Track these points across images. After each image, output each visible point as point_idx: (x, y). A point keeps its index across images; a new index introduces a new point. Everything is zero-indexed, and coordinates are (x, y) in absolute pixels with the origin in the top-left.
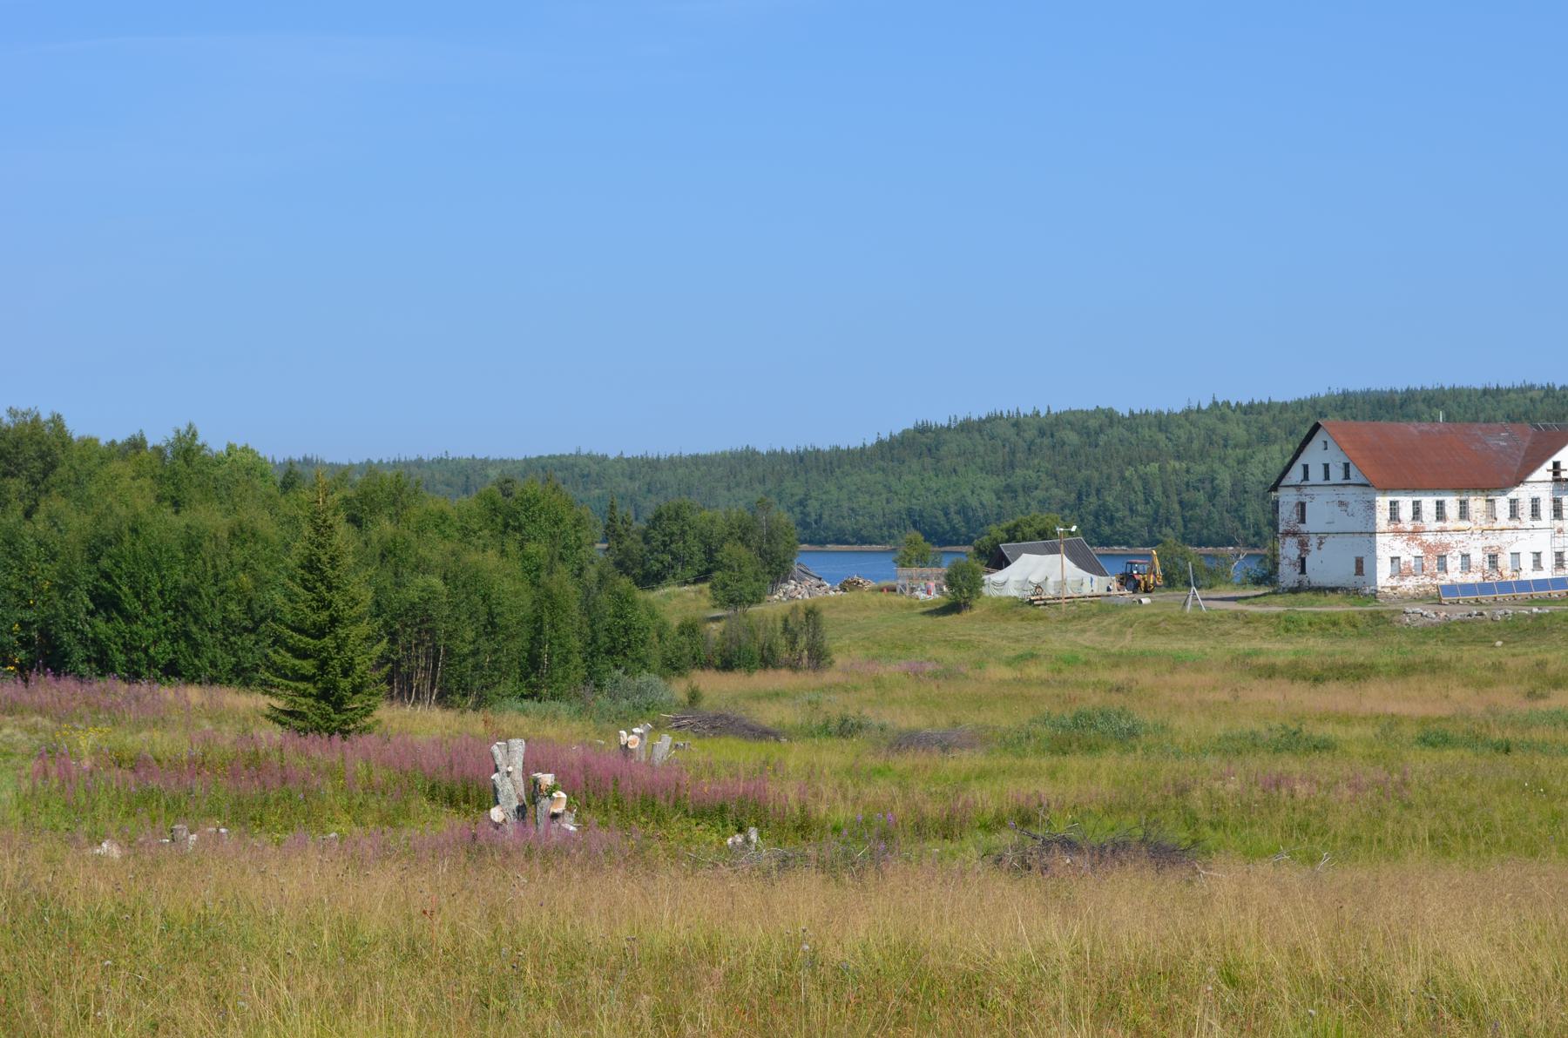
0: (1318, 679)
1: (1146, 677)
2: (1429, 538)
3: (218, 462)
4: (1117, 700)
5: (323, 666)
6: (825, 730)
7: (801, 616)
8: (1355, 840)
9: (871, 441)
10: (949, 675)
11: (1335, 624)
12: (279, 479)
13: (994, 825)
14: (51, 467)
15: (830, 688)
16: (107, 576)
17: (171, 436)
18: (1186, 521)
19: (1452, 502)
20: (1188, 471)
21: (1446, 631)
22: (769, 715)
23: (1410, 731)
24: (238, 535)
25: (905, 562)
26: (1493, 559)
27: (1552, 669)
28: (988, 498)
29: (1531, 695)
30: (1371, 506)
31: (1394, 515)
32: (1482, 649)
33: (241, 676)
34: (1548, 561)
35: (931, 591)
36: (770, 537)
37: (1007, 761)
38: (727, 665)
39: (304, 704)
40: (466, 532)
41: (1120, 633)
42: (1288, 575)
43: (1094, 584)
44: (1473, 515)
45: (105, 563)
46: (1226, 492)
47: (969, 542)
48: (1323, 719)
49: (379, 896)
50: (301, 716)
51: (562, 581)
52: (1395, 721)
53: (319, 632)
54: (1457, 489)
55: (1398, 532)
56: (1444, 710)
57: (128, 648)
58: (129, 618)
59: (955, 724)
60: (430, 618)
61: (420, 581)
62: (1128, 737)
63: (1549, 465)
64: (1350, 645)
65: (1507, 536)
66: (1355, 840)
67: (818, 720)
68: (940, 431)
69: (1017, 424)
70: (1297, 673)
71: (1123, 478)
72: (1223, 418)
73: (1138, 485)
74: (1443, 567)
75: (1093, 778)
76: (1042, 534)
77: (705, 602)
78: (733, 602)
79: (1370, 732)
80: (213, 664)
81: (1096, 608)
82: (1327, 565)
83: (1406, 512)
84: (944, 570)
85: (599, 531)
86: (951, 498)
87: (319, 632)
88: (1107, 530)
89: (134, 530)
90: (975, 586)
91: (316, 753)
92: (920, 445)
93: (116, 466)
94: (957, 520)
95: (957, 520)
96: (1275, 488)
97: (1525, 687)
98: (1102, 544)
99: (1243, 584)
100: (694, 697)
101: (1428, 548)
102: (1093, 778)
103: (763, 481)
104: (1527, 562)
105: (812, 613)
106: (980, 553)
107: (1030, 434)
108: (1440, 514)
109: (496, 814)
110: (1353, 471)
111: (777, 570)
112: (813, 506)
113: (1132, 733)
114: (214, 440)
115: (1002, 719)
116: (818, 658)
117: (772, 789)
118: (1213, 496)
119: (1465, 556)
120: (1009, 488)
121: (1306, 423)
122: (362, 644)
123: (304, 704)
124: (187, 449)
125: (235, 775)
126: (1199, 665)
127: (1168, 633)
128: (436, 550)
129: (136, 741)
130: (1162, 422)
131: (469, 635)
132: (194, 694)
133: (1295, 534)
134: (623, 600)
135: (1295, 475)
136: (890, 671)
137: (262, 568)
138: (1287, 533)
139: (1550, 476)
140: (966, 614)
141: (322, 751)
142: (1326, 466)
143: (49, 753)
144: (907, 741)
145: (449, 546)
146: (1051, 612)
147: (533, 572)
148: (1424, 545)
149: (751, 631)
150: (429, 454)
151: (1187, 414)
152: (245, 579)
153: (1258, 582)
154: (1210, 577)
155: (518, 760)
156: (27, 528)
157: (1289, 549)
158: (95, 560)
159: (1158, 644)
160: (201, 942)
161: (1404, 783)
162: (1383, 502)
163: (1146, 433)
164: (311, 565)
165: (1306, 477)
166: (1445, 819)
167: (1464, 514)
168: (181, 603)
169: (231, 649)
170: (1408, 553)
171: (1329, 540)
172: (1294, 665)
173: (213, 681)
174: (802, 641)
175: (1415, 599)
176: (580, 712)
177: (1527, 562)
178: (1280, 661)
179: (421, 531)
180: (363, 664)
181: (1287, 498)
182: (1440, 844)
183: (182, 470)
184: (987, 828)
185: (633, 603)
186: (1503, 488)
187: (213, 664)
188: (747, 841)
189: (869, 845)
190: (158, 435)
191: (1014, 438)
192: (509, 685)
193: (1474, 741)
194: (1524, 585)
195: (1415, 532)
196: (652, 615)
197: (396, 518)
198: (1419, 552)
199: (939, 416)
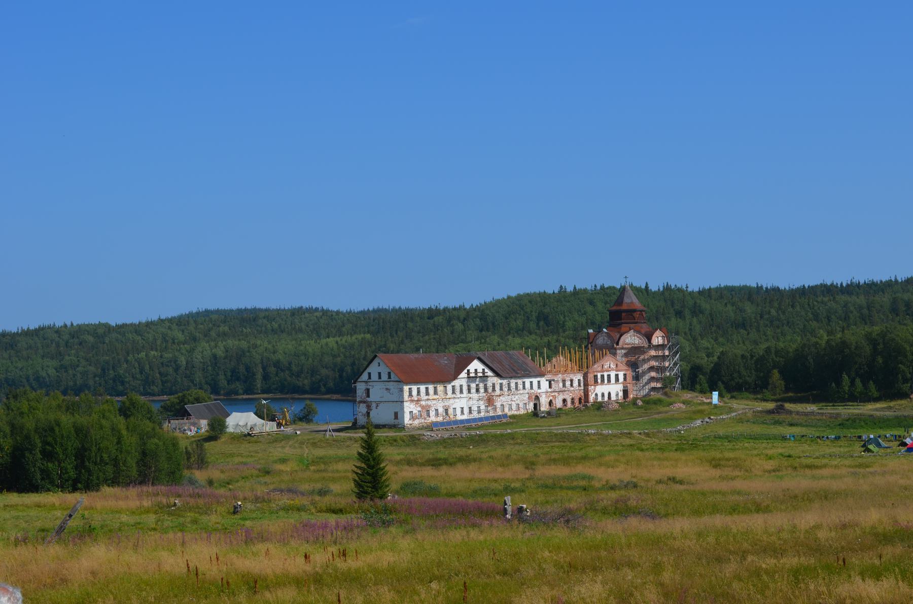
2: (423, 403)
11: (395, 441)
18: (163, 383)
19: (431, 388)
20: (161, 357)
26: (446, 411)
30: (402, 390)
31: (410, 395)
34: (466, 411)
44: (439, 393)
46: (183, 368)
54: (433, 382)
55: (412, 401)
63: (466, 371)
65: (451, 401)
68: (14, 336)
69: (58, 331)
71: (127, 361)
73: (137, 365)
81: (275, 439)
83: (415, 393)
86: (30, 372)
98: (118, 395)
101: (423, 407)
104: (458, 412)
107: (66, 337)
108: (427, 393)
110: (392, 376)
118: (177, 369)
119: (437, 410)
120: (62, 366)
133: (364, 402)
138: (360, 402)
139: (466, 376)
142: (380, 373)
163: (130, 336)
165: (370, 377)
167: (436, 393)
170: (416, 410)
171: (381, 405)
177: (458, 412)
186: (450, 381)
191: (57, 339)
194: (456, 422)
195: (418, 400)
198: (419, 409)
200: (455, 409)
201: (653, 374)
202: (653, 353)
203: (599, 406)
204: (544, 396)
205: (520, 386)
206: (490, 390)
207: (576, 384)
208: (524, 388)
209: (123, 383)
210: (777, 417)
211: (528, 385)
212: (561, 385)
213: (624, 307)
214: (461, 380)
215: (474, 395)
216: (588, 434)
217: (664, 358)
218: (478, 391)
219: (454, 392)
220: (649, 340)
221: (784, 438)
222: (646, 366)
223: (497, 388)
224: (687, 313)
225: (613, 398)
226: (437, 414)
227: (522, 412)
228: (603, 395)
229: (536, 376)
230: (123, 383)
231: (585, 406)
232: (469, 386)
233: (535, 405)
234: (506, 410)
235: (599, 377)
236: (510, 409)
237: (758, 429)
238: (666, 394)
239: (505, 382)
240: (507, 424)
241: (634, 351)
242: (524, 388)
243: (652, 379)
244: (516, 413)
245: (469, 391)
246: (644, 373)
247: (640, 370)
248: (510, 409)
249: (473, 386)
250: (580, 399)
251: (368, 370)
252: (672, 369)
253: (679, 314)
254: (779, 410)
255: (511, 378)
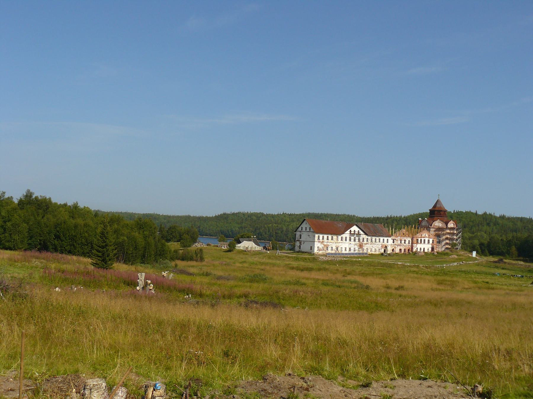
0: (302, 270)
1: (268, 268)
2: (325, 243)
3: (82, 210)
4: (262, 272)
5: (103, 254)
6: (203, 274)
7: (199, 250)
8: (312, 304)
9: (214, 216)
10: (227, 265)
12: (94, 214)
13: (240, 297)
14: (48, 208)
15: (205, 265)
16: (58, 232)
17: (73, 204)
19: (330, 237)
21: (327, 262)
22: (192, 270)
23: (321, 282)
24: (86, 225)
25: (220, 241)
26: (337, 248)
27: (348, 271)
28: (237, 229)
29: (344, 276)
30: (314, 236)
31: (319, 239)
32: (334, 266)
33: (84, 254)
34: (348, 249)
35: (225, 247)
36: (193, 233)
37: (240, 283)
38: (183, 259)
39: (99, 262)
40: (132, 228)
41: (263, 258)
42: (297, 249)
43: (258, 248)
45: (58, 229)
47: (233, 237)
48: (303, 278)
49: (119, 306)
50: (98, 264)
51: (151, 240)
52: (318, 280)
53: (103, 247)
54: (331, 234)
55: (319, 242)
56: (327, 278)
57: (61, 247)
58: (62, 241)
59: (229, 275)
60: (123, 245)
61: (122, 238)
62: (264, 280)
63: (349, 230)
64: (308, 264)
65: (340, 244)
66: (312, 304)
67: (202, 272)
69: (244, 214)
70: (298, 269)
72: (285, 216)
73: (267, 229)
74: (327, 249)
75: (258, 288)
76: (248, 237)
77: (179, 246)
78: (184, 246)
79: (312, 282)
80: (78, 252)
82: (305, 247)
83: (321, 238)
84: (228, 243)
85: (158, 230)
87: (103, 247)
88: (260, 237)
89: (64, 223)
90: (234, 247)
91: (101, 273)
92: (224, 217)
93: (61, 209)
94: (230, 233)
95: (230, 233)
96: (296, 231)
97: (342, 274)
99: (287, 250)
100: (176, 265)
101: (325, 245)
102: (258, 288)
103: (191, 222)
104: (344, 249)
105: (201, 250)
106: (235, 240)
108: (328, 239)
109: (138, 288)
111: (194, 241)
112: (201, 228)
113: (265, 279)
114: (81, 205)
115: (239, 274)
116: (202, 259)
117: (194, 286)
118: (282, 232)
119: (332, 247)
121: (302, 218)
122: (111, 250)
123: (99, 262)
124: (76, 206)
125: (84, 276)
126: (279, 266)
127: (272, 259)
128: (126, 231)
129: (64, 267)
130: (273, 216)
131: (131, 250)
132: (75, 258)
134: (163, 245)
135: (300, 229)
136: (217, 263)
137: (90, 232)
140: (232, 252)
141: (101, 272)
143: (45, 268)
144: (219, 278)
145: (128, 231)
146: (249, 253)
147: (145, 237)
148: (325, 245)
149: (188, 253)
150: (123, 211)
151: (278, 215)
152: (86, 234)
153: (290, 250)
154: (282, 248)
155: (143, 277)
156: (42, 220)
157: (298, 244)
158: (56, 228)
159: (270, 261)
160: (81, 313)
161: (321, 293)
162: (317, 236)
164: (102, 233)
166: (329, 300)
167: (332, 239)
168: (73, 238)
169: (82, 249)
170: (321, 246)
171: (305, 243)
172: (297, 267)
173: (78, 255)
174: (199, 256)
175: (322, 255)
176: (153, 267)
177: (344, 249)
178: (295, 266)
179: (123, 227)
180: (111, 255)
181: (298, 234)
182: (328, 306)
183: (74, 211)
184: (238, 298)
185: (165, 245)
187: (78, 252)
188: (189, 297)
189: (215, 301)
190: (70, 203)
192: (139, 260)
193: (333, 285)
194: (343, 254)
196: (168, 248)
197: (118, 224)
199: (228, 212)
200: (342, 248)
201: (448, 241)
202: (448, 231)
203: (415, 253)
204: (390, 246)
205: (378, 241)
206: (361, 241)
207: (407, 242)
208: (379, 242)
209: (261, 235)
210: (497, 264)
211: (381, 240)
212: (399, 242)
213: (437, 209)
214: (347, 234)
215: (352, 242)
216: (397, 264)
217: (453, 234)
218: (355, 240)
219: (342, 240)
220: (447, 225)
221: (494, 274)
222: (444, 237)
223: (365, 240)
224: (492, 224)
225: (426, 251)
226: (332, 249)
227: (377, 253)
228: (421, 249)
229: (386, 237)
230: (261, 235)
231: (411, 253)
232: (350, 238)
233: (385, 250)
234: (369, 251)
235: (419, 239)
236: (371, 251)
237: (484, 269)
238: (451, 251)
239: (369, 238)
240: (367, 257)
241: (439, 229)
242: (379, 242)
243: (447, 244)
244: (374, 253)
245: (350, 240)
246: (443, 240)
247: (441, 239)
248: (371, 251)
249: (352, 238)
250: (409, 250)
251: (301, 226)
252: (457, 240)
253: (488, 224)
254: (501, 260)
255: (373, 236)
